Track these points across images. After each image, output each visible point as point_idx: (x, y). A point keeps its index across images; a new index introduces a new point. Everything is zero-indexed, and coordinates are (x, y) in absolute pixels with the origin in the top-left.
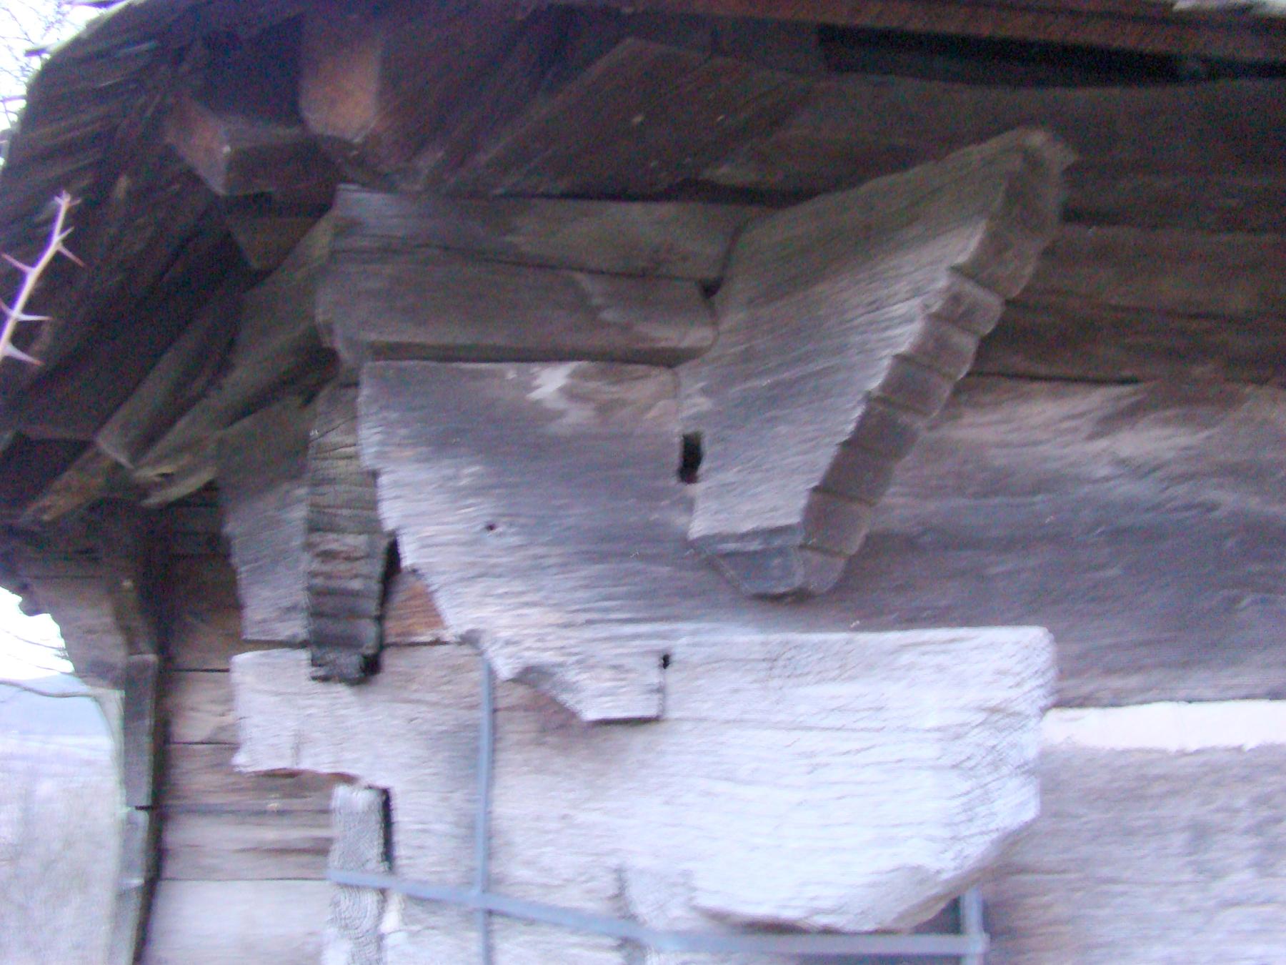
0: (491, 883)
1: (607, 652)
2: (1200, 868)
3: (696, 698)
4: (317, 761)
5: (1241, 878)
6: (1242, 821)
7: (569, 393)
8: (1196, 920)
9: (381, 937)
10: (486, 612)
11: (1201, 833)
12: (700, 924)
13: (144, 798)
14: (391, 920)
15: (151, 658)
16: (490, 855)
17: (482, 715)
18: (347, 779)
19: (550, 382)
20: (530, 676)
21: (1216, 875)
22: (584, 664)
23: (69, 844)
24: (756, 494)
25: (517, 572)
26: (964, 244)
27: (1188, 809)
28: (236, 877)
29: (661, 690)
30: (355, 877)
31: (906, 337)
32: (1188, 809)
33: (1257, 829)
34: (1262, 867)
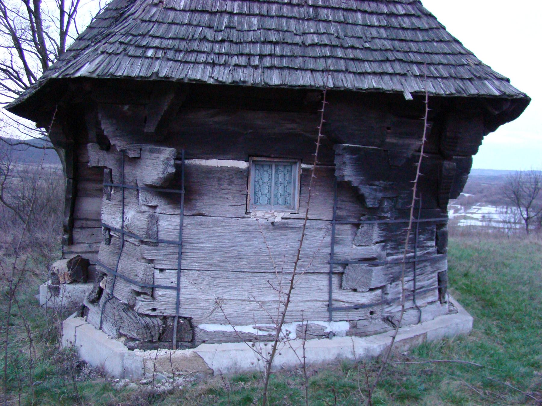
0: (124, 183)
1: (133, 148)
2: (219, 184)
3: (146, 155)
4: (101, 164)
5: (226, 186)
6: (227, 177)
7: (128, 109)
8: (218, 191)
9: (111, 194)
10: (116, 142)
11: (220, 179)
12: (144, 186)
13: (72, 176)
14: (113, 192)
15: (72, 141)
16: (124, 178)
17: (123, 157)
18: (106, 167)
19: (126, 108)
20: (122, 151)
21: (221, 185)
22: (129, 150)
23: (49, 200)
24: (150, 128)
25: (121, 137)
26: (172, 96)
27: (218, 175)
28: (95, 196)
29: (140, 154)
30: (106, 184)
31: (166, 108)
32: (218, 175)
33: (229, 179)
34: (229, 185)
